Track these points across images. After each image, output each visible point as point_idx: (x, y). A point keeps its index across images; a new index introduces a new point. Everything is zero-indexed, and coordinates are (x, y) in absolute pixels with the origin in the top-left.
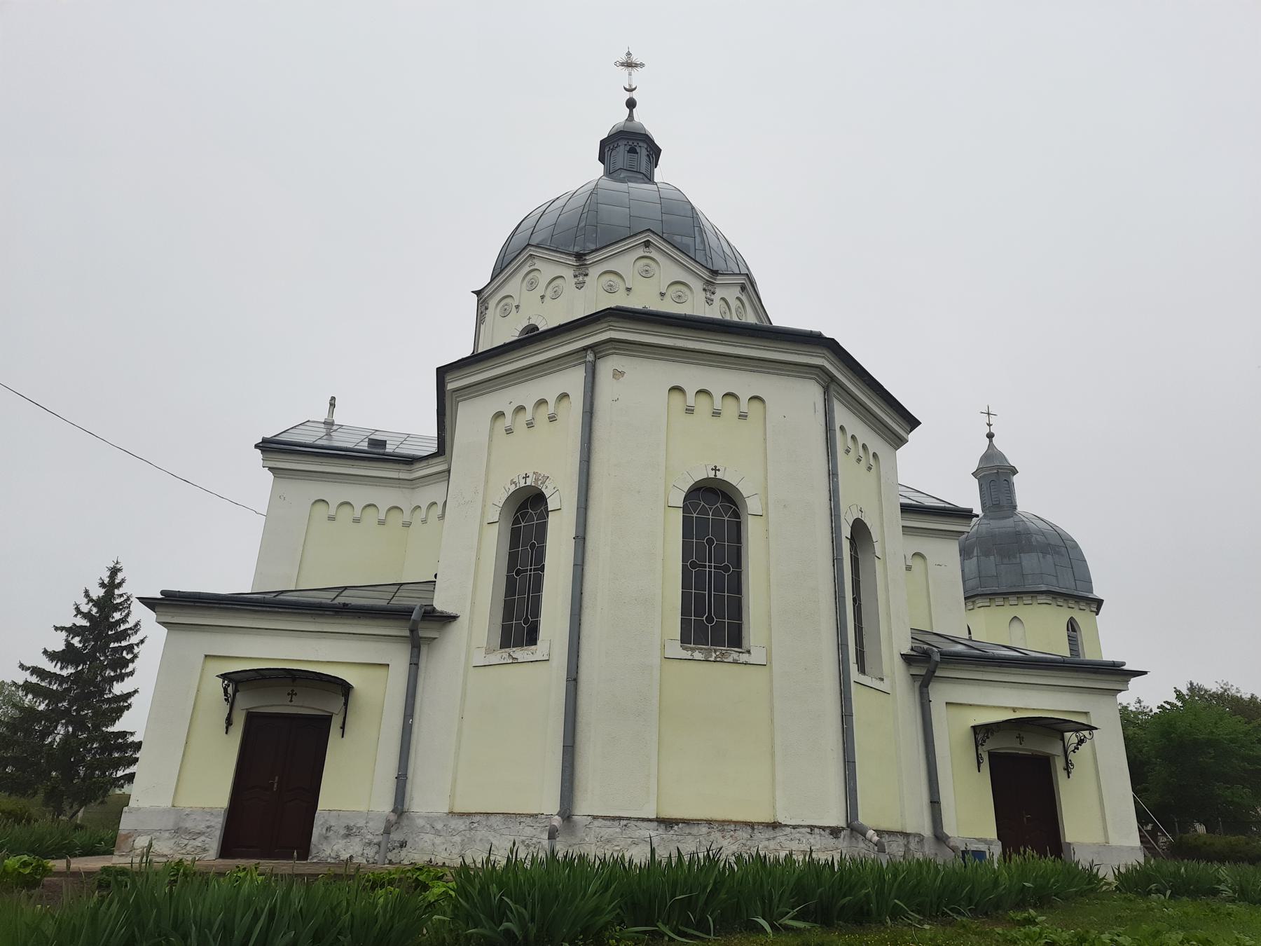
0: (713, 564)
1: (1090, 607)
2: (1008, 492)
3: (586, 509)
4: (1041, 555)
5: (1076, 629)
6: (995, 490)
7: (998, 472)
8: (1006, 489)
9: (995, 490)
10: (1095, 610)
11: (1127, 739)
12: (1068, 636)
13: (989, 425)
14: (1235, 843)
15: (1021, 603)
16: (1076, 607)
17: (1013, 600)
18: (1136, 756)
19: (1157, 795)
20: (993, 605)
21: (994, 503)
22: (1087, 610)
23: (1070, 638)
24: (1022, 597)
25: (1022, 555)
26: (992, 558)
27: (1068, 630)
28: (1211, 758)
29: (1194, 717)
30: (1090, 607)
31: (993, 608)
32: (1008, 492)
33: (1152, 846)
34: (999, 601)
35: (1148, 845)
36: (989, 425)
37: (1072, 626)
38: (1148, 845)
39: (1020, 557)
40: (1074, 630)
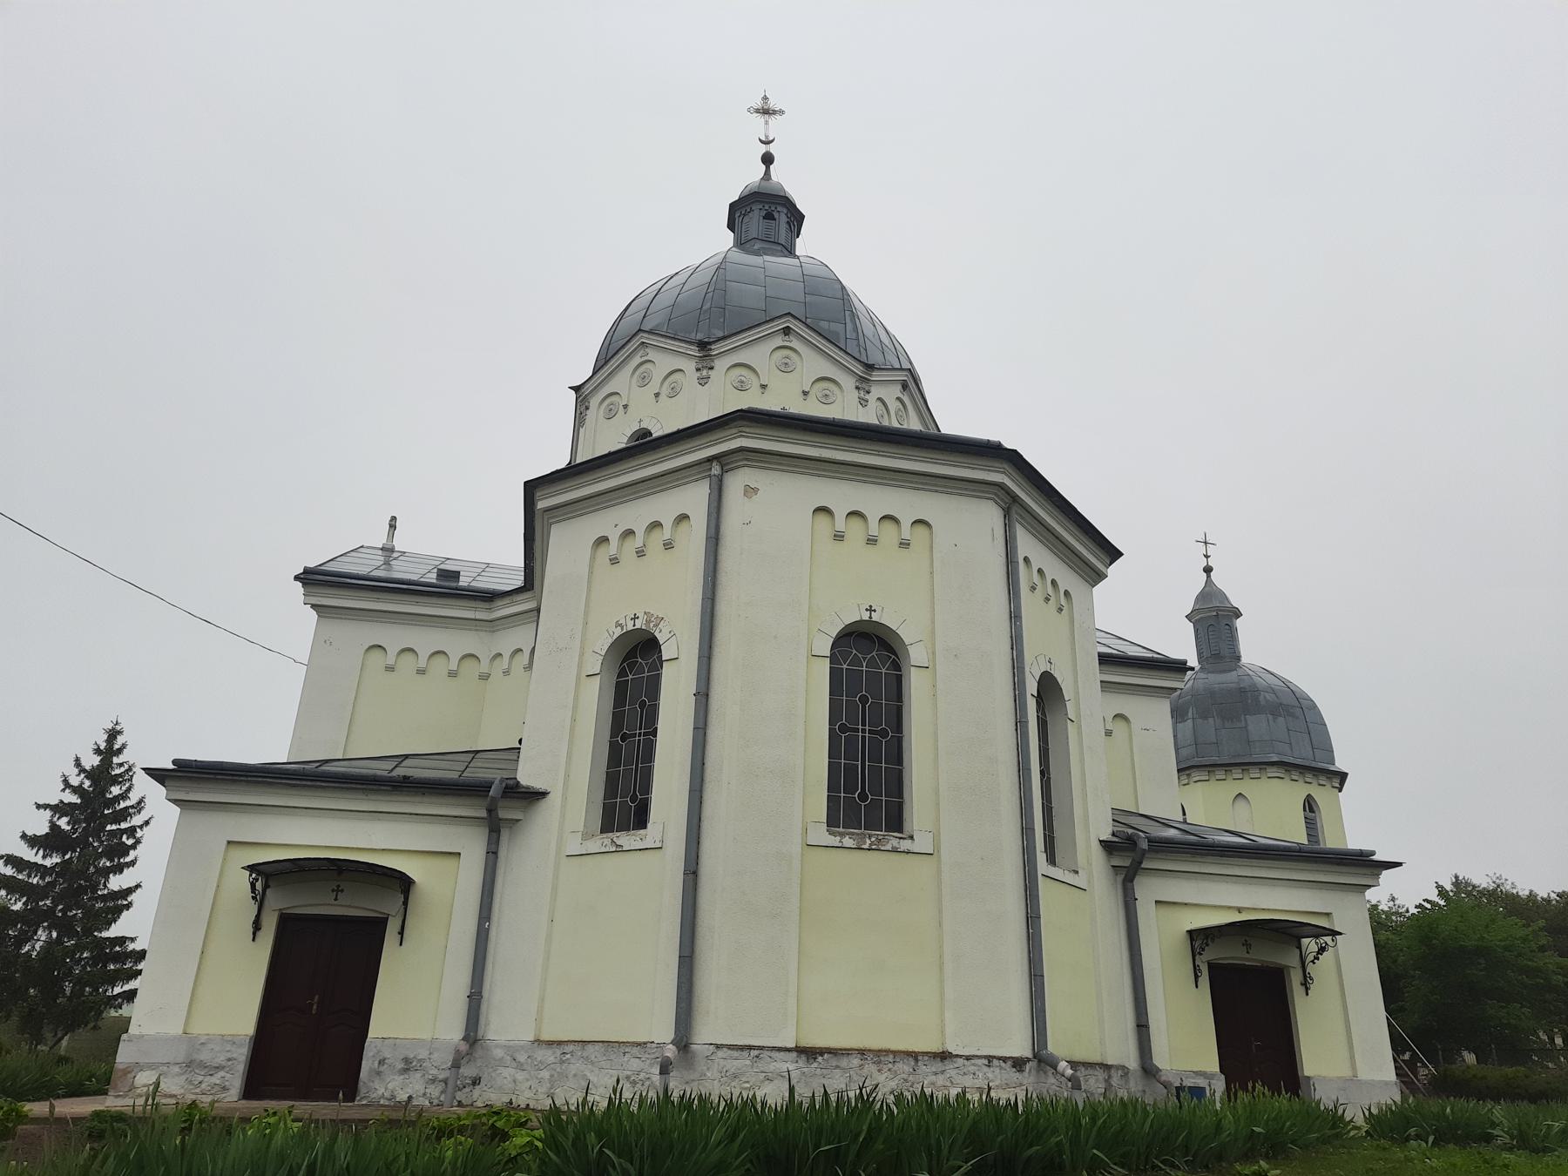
5: (1315, 809)
7: (1217, 615)
10: (1338, 786)
13: (1207, 557)
15: (1246, 777)
17: (1237, 773)
20: (1213, 778)
22: (1328, 786)
23: (1308, 821)
26: (1211, 720)
27: (1305, 810)
28: (1481, 970)
31: (1213, 783)
33: (1404, 1072)
34: (1220, 774)
36: (1207, 557)
37: (1310, 805)
40: (1312, 810)
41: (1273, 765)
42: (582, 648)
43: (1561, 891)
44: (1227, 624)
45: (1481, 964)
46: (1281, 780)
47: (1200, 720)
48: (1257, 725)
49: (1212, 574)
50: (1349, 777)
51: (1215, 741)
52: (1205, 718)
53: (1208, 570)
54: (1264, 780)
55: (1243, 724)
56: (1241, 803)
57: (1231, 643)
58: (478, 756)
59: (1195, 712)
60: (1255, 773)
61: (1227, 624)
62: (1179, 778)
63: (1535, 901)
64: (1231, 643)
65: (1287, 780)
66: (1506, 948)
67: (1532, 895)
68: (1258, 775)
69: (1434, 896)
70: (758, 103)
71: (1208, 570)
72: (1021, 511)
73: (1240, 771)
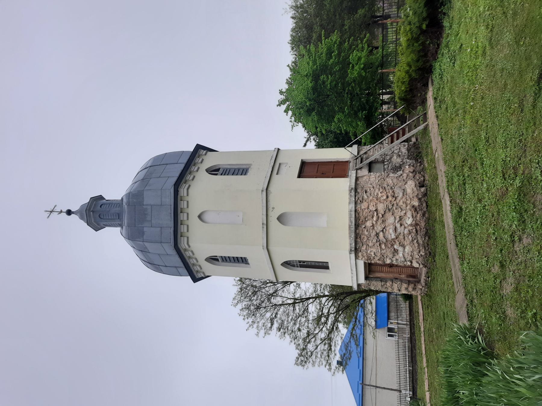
0: (298, 264)
1: (202, 155)
3: (301, 266)
5: (217, 168)
7: (93, 211)
10: (205, 152)
11: (332, 147)
12: (221, 175)
13: (61, 212)
14: (409, 34)
17: (182, 217)
20: (187, 234)
22: (204, 157)
23: (227, 173)
24: (181, 209)
26: (145, 229)
27: (216, 174)
29: (412, 197)
30: (202, 155)
33: (396, 134)
35: (401, 133)
36: (61, 212)
37: (214, 171)
39: (147, 205)
40: (218, 170)
41: (178, 191)
43: (290, 48)
44: (101, 207)
47: (145, 236)
48: (150, 199)
49: (73, 210)
50: (284, 111)
51: (159, 229)
52: (143, 233)
53: (69, 212)
54: (189, 199)
55: (149, 207)
56: (206, 217)
57: (113, 205)
60: (182, 205)
61: (101, 207)
62: (202, 278)
64: (113, 205)
69: (284, 107)
70: (47, 214)
71: (69, 212)
72: (49, 214)
73: (182, 214)
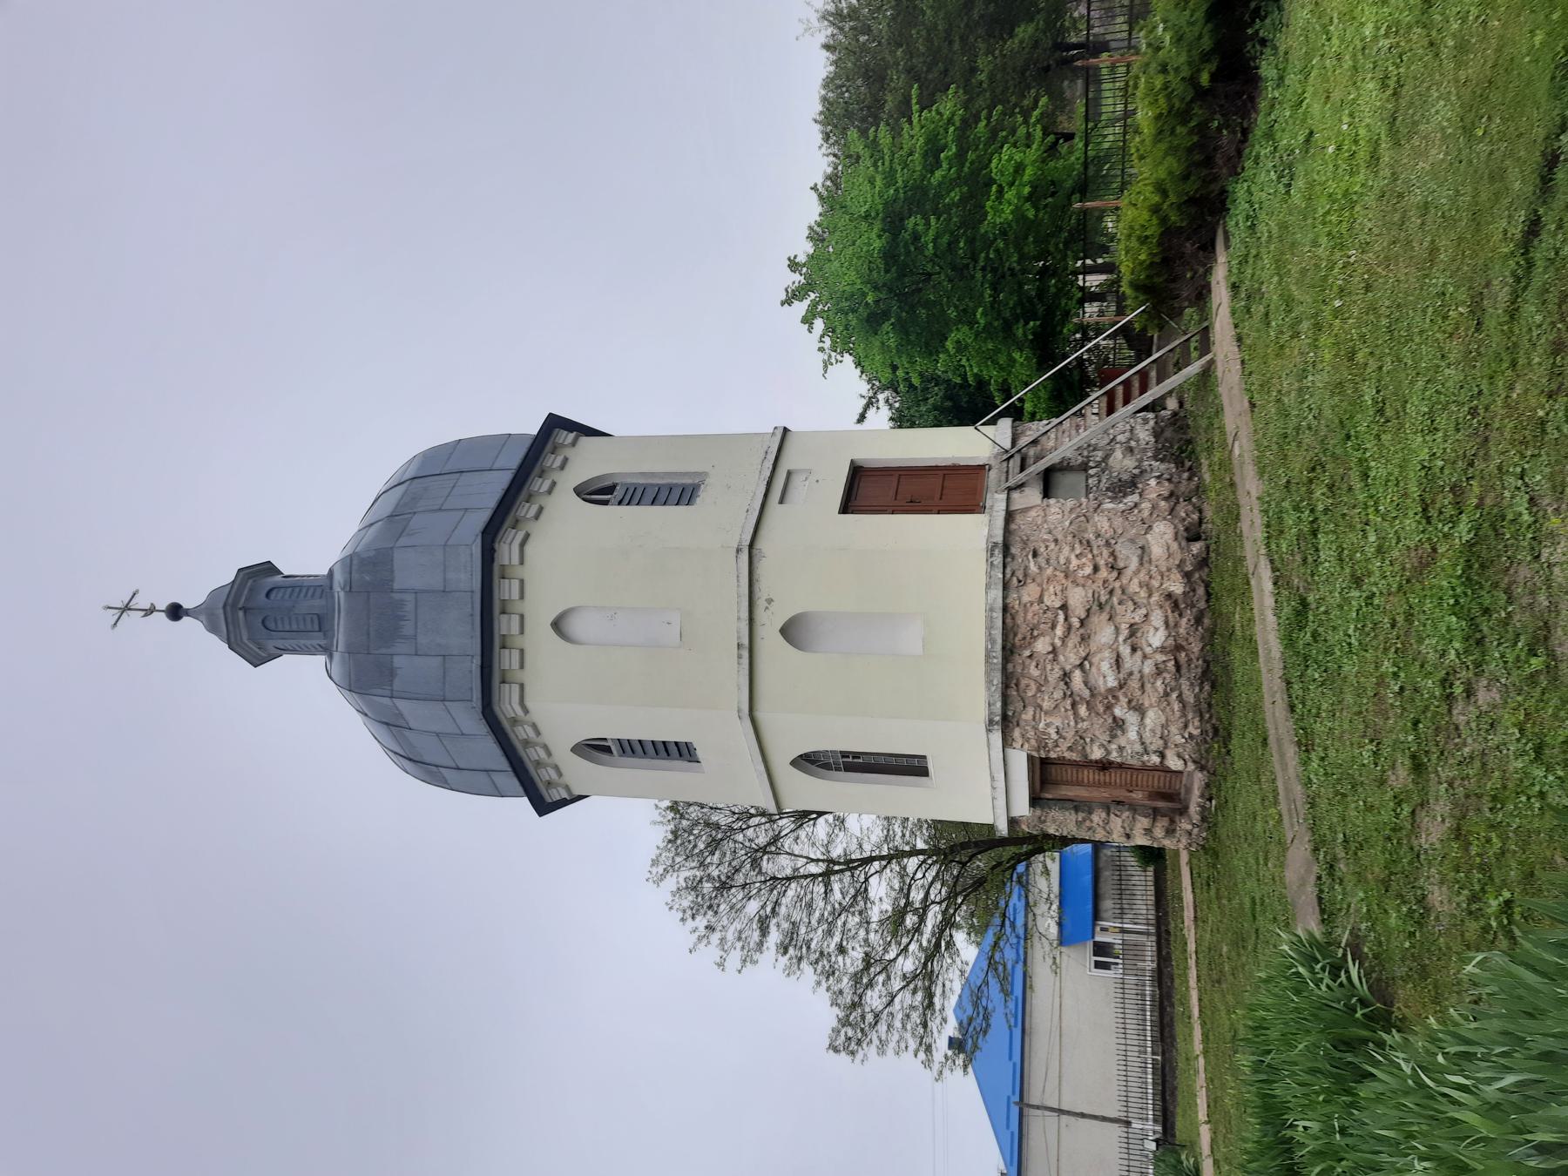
2: (297, 590)
3: (849, 768)
4: (403, 541)
5: (608, 483)
6: (286, 622)
7: (245, 609)
8: (287, 597)
9: (286, 622)
10: (572, 436)
12: (620, 503)
13: (150, 611)
14: (1162, 101)
15: (518, 607)
16: (556, 476)
17: (506, 625)
18: (935, 408)
19: (1016, 355)
21: (317, 628)
22: (569, 452)
25: (396, 586)
26: (398, 661)
27: (605, 503)
28: (928, 224)
30: (563, 445)
31: (528, 676)
32: (297, 590)
33: (1120, 389)
34: (507, 660)
36: (150, 611)
37: (598, 492)
38: (1153, 374)
40: (610, 490)
42: (416, 623)
45: (916, 224)
46: (531, 540)
48: (411, 573)
49: (185, 606)
52: (392, 673)
53: (175, 612)
54: (526, 572)
55: (409, 597)
57: (304, 590)
58: (437, 507)
59: (379, 691)
60: (506, 590)
61: (268, 595)
63: (836, 75)
65: (535, 528)
66: (890, 178)
67: (828, 83)
68: (516, 584)
71: (175, 612)
73: (504, 618)
